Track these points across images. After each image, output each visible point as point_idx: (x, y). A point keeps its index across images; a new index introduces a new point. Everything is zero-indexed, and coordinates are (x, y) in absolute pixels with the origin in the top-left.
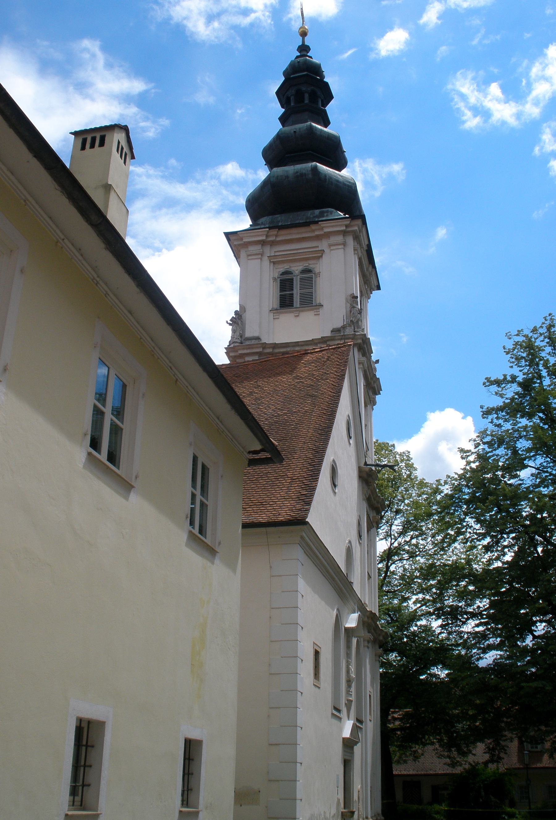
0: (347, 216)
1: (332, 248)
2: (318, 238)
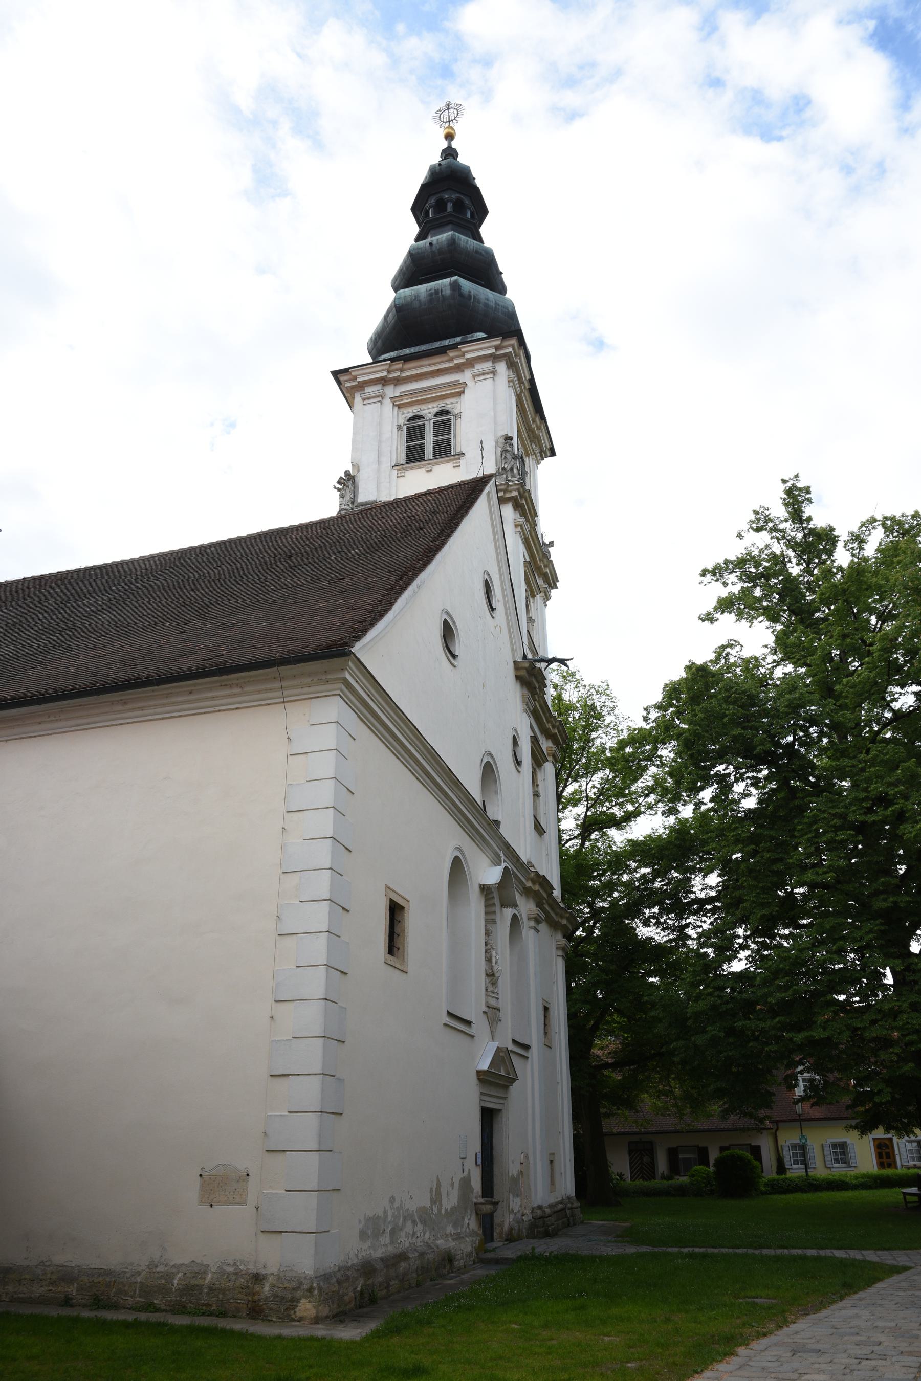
1: (477, 379)
2: (459, 368)
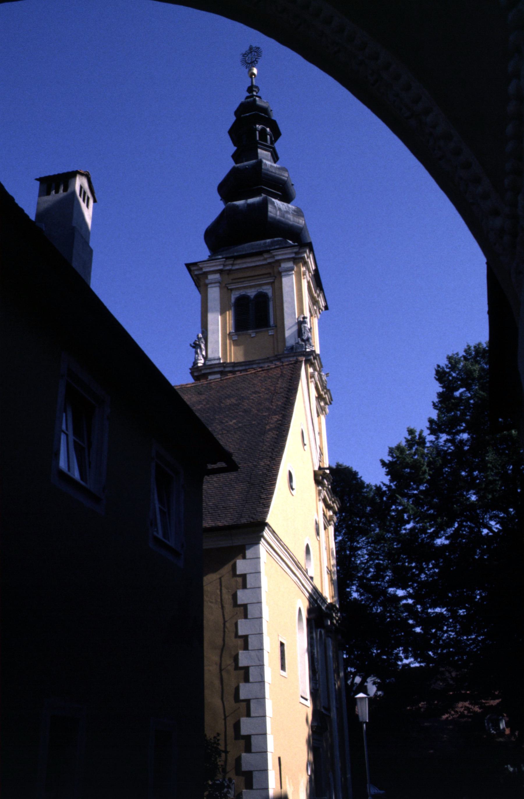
0: (296, 244)
